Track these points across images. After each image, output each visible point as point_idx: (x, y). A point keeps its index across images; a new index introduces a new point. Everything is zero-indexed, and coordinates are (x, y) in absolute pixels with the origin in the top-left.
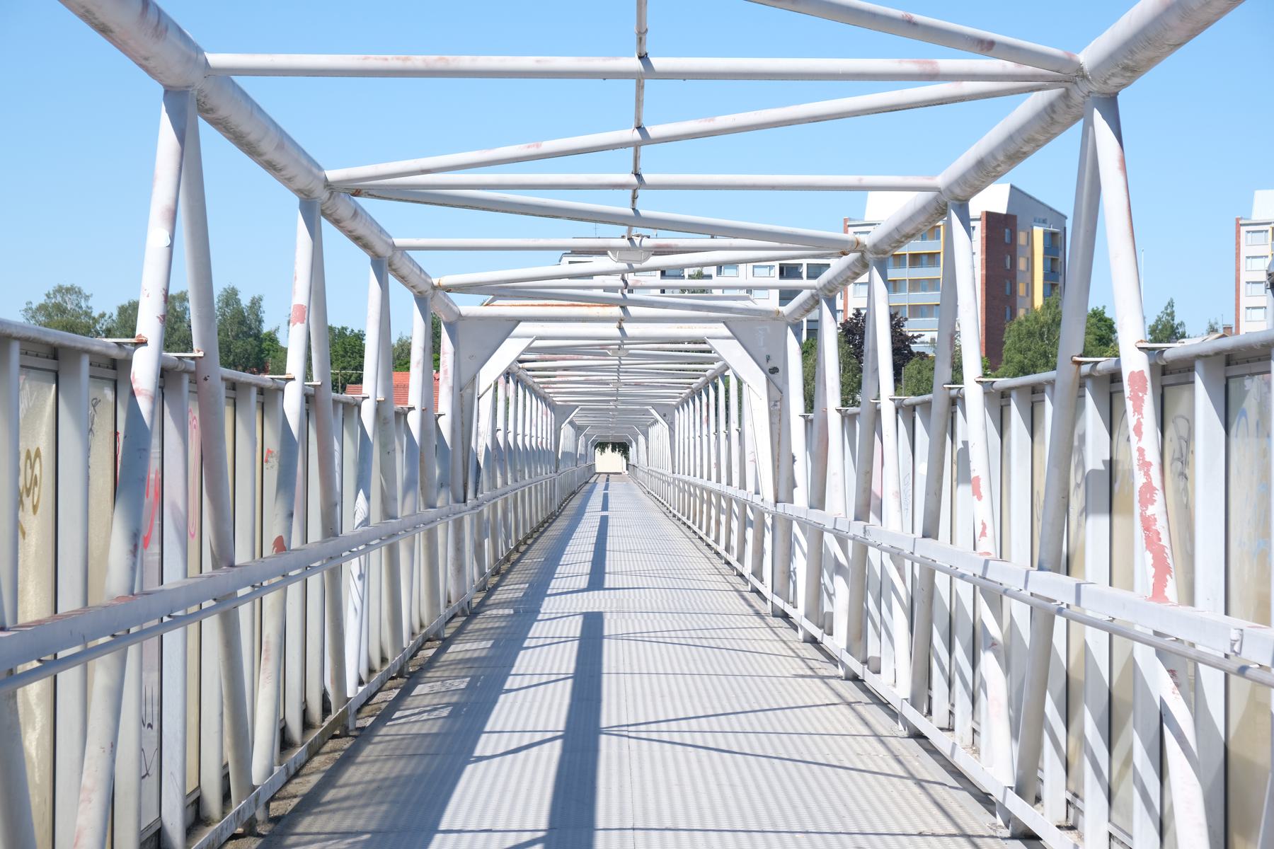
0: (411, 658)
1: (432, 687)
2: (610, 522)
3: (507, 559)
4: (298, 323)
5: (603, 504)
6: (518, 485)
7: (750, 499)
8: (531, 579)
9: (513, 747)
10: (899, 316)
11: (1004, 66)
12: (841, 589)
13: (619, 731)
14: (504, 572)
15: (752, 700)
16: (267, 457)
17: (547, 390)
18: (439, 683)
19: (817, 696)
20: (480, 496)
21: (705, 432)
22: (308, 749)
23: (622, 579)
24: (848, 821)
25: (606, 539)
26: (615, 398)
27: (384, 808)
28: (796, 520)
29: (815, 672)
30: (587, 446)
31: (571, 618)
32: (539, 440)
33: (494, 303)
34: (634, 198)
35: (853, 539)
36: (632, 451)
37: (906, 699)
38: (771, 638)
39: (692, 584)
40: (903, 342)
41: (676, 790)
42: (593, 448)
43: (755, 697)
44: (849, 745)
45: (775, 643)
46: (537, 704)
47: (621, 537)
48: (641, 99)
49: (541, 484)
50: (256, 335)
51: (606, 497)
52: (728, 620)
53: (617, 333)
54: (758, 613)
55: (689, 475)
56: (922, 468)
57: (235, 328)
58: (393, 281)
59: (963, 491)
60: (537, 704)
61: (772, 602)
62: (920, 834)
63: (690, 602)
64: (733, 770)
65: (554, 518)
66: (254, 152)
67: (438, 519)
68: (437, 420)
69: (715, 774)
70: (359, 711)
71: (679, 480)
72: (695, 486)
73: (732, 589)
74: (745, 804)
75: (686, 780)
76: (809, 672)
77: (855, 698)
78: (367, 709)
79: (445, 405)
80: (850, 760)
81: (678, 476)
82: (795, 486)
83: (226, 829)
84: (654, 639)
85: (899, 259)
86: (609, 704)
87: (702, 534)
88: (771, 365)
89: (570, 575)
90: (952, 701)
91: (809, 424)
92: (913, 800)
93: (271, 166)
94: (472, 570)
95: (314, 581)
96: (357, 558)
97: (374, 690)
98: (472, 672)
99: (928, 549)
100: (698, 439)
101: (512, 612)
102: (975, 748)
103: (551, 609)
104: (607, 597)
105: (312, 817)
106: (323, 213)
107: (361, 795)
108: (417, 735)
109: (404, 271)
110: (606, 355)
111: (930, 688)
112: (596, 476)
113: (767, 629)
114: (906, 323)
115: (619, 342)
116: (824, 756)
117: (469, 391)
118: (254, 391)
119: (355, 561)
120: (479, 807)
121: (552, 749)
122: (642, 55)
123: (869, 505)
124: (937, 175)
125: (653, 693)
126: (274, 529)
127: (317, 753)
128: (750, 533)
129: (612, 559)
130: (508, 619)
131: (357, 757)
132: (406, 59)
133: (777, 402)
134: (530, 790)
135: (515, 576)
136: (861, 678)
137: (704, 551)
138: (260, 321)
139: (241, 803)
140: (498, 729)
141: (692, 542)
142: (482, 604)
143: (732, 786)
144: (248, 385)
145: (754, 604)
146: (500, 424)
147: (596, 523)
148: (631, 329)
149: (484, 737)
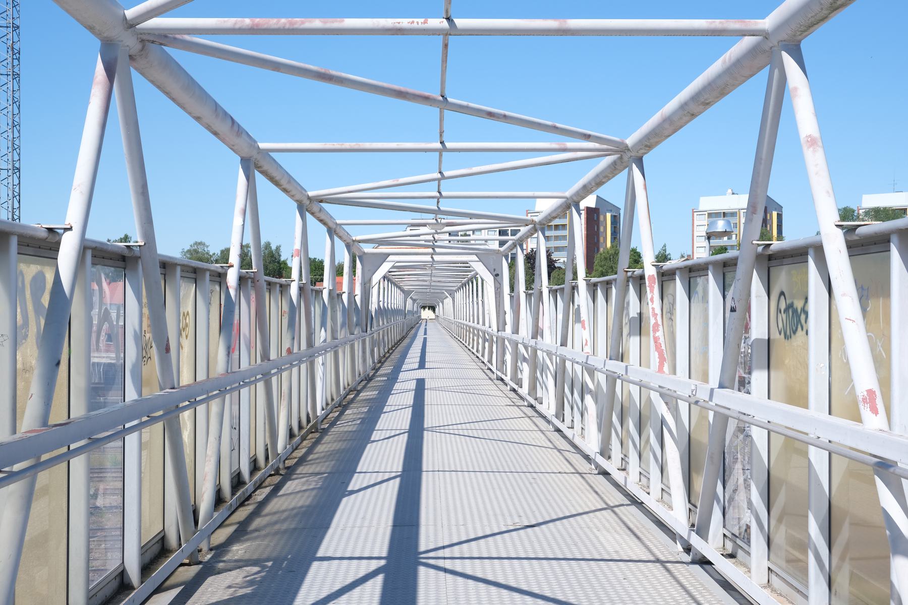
3: (384, 356)
6: (388, 324)
12: (526, 368)
13: (432, 429)
15: (488, 416)
17: (401, 284)
20: (373, 329)
21: (468, 301)
24: (529, 467)
27: (333, 463)
30: (417, 308)
32: (398, 305)
34: (438, 202)
35: (531, 347)
36: (437, 310)
50: (279, 262)
51: (426, 329)
53: (431, 259)
54: (490, 379)
56: (560, 316)
58: (336, 239)
59: (578, 326)
62: (560, 473)
69: (473, 447)
70: (322, 421)
74: (486, 460)
76: (512, 404)
78: (326, 421)
79: (358, 291)
80: (530, 441)
85: (550, 227)
87: (467, 345)
88: (496, 273)
92: (556, 458)
93: (285, 191)
94: (369, 361)
98: (370, 404)
99: (563, 351)
100: (465, 305)
101: (386, 379)
102: (583, 436)
106: (307, 210)
109: (341, 234)
111: (563, 410)
114: (552, 254)
117: (368, 285)
118: (278, 286)
119: (320, 358)
121: (404, 437)
126: (286, 345)
127: (305, 439)
128: (487, 344)
132: (343, 144)
136: (534, 406)
138: (280, 256)
142: (374, 375)
143: (480, 452)
144: (276, 283)
146: (381, 299)
147: (422, 340)
148: (436, 258)
149: (375, 432)
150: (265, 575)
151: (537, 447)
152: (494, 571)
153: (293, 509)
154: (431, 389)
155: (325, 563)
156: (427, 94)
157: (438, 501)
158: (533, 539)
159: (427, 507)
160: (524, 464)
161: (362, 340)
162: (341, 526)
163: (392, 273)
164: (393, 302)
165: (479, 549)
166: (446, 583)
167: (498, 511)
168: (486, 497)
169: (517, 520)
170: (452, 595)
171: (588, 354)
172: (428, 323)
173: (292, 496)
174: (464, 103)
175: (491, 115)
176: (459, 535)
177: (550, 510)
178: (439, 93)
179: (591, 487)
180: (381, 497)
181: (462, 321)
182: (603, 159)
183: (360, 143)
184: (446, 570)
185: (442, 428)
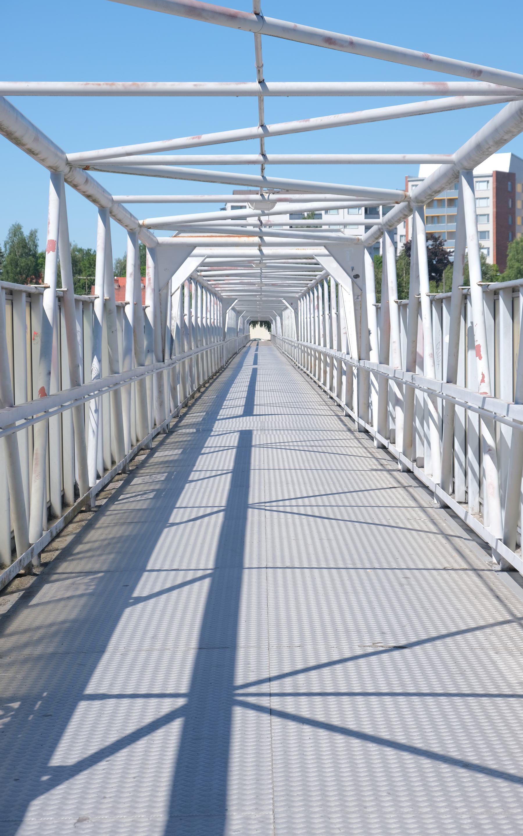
0: (131, 461)
1: (144, 479)
2: (259, 372)
3: (192, 397)
4: (51, 252)
5: (254, 360)
6: (199, 349)
7: (344, 357)
8: (207, 409)
9: (193, 517)
10: (441, 239)
11: (489, 86)
12: (399, 414)
13: (260, 506)
14: (190, 405)
15: (344, 486)
16: (34, 337)
17: (217, 289)
18: (148, 477)
19: (384, 482)
20: (173, 357)
21: (316, 315)
22: (64, 520)
23: (265, 409)
24: (400, 561)
25: (255, 383)
26: (260, 293)
27: (112, 556)
28: (371, 371)
29: (384, 467)
30: (244, 324)
31: (232, 434)
32: (212, 320)
33: (180, 235)
34: (263, 169)
35: (405, 383)
36: (273, 326)
37: (438, 484)
38: (356, 446)
39: (308, 411)
40: (444, 255)
41: (293, 543)
42: (248, 324)
43: (345, 483)
44: (403, 513)
45: (359, 449)
46: (208, 490)
47: (265, 381)
48: (262, 108)
49: (214, 349)
50: (34, 255)
51: (256, 356)
52: (330, 434)
53: (257, 252)
54: (349, 430)
55: (307, 341)
56: (447, 339)
57: (20, 251)
58: (113, 222)
59: (471, 354)
60: (208, 490)
61: (358, 423)
62: (445, 569)
63: (307, 423)
64: (329, 530)
65: (223, 369)
66: (20, 143)
67: (146, 373)
68: (144, 310)
69: (319, 532)
70: (97, 495)
71: (301, 345)
72: (311, 349)
73: (333, 414)
74: (337, 551)
75: (300, 536)
76: (380, 467)
77: (408, 484)
78: (103, 494)
79: (149, 301)
80: (403, 522)
81: (301, 343)
82: (371, 349)
83: (13, 571)
84: (283, 447)
85: (430, 205)
86: (254, 489)
87: (316, 379)
88: (355, 273)
89: (232, 406)
90: (467, 485)
91: (379, 310)
92: (441, 547)
93: (31, 152)
94: (169, 403)
95: (67, 414)
96: (94, 400)
97: (106, 482)
98: (168, 470)
99: (450, 390)
100: (312, 319)
101: (195, 430)
102: (480, 514)
103: (219, 429)
104: (255, 420)
105: (68, 562)
106: (66, 181)
107: (98, 548)
108: (133, 510)
109: (120, 216)
110: (252, 267)
111: (454, 477)
112: (251, 342)
113: (355, 440)
114: (445, 243)
115: (260, 259)
116: (387, 520)
117: (165, 291)
118: (24, 295)
119: (93, 401)
120: (171, 555)
121: (217, 518)
122: (261, 81)
123: (415, 362)
124: (453, 153)
125: (281, 482)
126: (39, 384)
127: (71, 522)
128: (344, 378)
129: (258, 396)
130: (192, 435)
131: (96, 524)
132: (113, 84)
133: (359, 296)
134: (203, 544)
135: (197, 407)
136: (412, 470)
137: (317, 390)
138: (36, 246)
139: (22, 554)
140: (184, 506)
141: (310, 384)
142: (176, 426)
143: (329, 540)
144: (20, 292)
145: (347, 424)
146: (186, 312)
147: (250, 373)
148: (267, 251)
149: (175, 510)
150: (9, 722)
151: (413, 532)
152: (341, 712)
153: (51, 625)
154: (260, 446)
155: (97, 704)
156: (233, 10)
157: (264, 612)
158: (401, 665)
159: (248, 621)
160: (393, 556)
161: (158, 373)
162: (121, 648)
163: (203, 273)
164: (204, 315)
165: (321, 681)
166: (271, 730)
167: (351, 626)
168: (334, 606)
169: (378, 638)
170: (280, 747)
171: (485, 396)
172: (259, 347)
173: (50, 606)
174: (290, 24)
175: (330, 41)
176: (293, 661)
177: (428, 624)
178: (252, 9)
179: (491, 590)
180: (181, 606)
181: (308, 344)
182: (508, 104)
183: (139, 83)
184: (271, 712)
185: (274, 504)
